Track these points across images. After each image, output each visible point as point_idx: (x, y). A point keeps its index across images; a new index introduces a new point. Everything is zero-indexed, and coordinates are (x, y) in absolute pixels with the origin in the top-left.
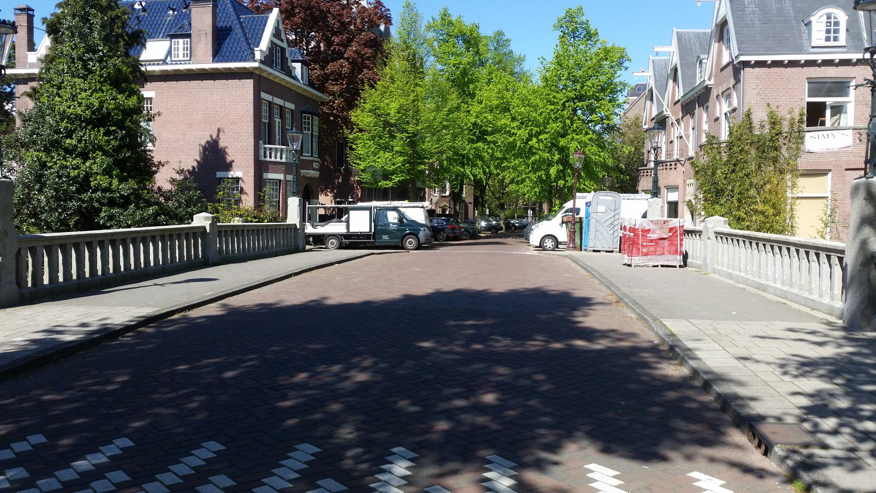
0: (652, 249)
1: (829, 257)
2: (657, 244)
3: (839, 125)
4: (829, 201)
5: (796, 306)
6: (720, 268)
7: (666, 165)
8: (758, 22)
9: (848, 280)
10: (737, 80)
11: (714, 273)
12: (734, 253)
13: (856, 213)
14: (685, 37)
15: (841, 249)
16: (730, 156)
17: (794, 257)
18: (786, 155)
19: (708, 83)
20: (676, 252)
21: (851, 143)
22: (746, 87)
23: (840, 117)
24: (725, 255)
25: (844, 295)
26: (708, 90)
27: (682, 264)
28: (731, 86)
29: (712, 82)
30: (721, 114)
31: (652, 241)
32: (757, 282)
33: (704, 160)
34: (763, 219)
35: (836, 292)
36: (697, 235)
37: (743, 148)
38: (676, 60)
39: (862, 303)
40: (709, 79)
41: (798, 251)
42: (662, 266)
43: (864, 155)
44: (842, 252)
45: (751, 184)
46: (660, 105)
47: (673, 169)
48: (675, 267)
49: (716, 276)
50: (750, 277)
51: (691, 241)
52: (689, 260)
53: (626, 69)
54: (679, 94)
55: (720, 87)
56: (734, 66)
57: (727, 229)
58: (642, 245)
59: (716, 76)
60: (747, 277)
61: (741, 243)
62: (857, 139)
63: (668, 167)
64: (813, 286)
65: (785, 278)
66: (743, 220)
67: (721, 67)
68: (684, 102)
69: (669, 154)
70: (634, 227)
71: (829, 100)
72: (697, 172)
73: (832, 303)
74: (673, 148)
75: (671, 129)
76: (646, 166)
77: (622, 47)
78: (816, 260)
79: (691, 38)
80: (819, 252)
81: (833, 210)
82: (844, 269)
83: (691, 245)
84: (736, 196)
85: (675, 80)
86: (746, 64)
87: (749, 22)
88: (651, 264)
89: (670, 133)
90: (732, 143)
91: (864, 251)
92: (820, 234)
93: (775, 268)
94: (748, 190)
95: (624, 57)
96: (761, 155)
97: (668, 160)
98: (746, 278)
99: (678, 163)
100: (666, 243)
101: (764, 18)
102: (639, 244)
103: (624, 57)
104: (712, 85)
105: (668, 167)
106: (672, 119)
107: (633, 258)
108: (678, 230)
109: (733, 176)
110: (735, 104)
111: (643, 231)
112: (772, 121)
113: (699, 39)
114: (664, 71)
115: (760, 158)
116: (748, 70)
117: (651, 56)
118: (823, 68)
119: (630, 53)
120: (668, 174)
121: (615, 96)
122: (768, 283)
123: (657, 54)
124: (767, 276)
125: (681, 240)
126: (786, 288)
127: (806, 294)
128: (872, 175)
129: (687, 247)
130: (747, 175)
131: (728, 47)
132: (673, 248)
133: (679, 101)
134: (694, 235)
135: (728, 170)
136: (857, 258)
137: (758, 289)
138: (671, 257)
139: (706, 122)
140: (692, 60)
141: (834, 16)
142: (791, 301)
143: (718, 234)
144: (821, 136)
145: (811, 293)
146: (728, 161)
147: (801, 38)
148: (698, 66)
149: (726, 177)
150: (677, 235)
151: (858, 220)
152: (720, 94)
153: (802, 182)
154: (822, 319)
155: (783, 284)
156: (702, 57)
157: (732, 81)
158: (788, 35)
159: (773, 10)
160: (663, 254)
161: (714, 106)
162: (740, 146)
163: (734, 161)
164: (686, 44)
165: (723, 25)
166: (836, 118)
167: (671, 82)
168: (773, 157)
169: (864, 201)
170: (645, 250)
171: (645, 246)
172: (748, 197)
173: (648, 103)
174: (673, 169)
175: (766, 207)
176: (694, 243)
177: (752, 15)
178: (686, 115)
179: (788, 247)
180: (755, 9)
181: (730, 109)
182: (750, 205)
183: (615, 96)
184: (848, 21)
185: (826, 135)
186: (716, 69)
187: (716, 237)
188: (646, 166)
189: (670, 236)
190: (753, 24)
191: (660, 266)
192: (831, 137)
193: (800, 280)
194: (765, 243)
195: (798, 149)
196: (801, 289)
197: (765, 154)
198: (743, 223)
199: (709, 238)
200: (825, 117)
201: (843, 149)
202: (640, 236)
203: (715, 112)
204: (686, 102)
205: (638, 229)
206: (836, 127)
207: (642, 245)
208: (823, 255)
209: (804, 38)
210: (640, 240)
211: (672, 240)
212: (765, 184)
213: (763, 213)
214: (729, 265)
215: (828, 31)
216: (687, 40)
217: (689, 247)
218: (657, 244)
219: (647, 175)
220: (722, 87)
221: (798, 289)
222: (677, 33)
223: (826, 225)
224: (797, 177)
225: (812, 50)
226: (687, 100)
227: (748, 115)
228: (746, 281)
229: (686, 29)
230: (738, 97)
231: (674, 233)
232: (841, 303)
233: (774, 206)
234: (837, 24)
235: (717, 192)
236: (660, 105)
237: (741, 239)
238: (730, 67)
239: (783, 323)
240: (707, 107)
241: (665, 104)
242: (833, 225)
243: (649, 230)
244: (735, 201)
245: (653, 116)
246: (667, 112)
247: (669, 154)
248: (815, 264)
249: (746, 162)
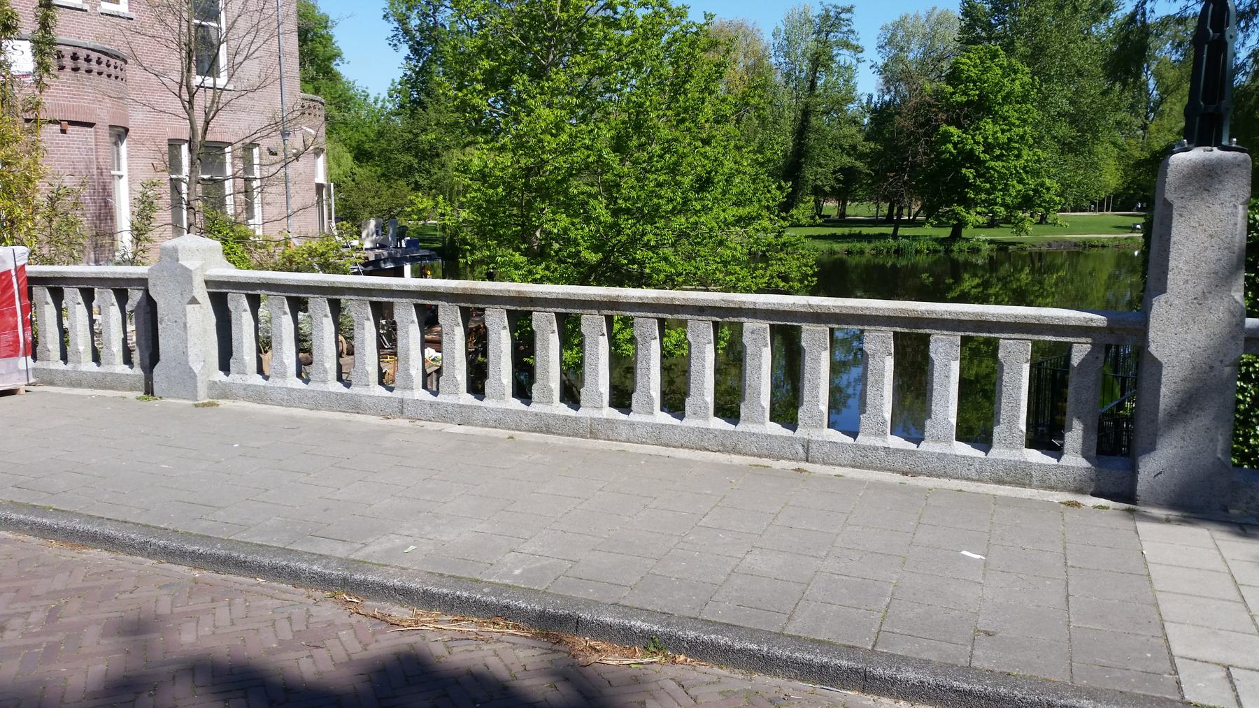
9: (1239, 147)
108: (14, 279)
150: (13, 296)
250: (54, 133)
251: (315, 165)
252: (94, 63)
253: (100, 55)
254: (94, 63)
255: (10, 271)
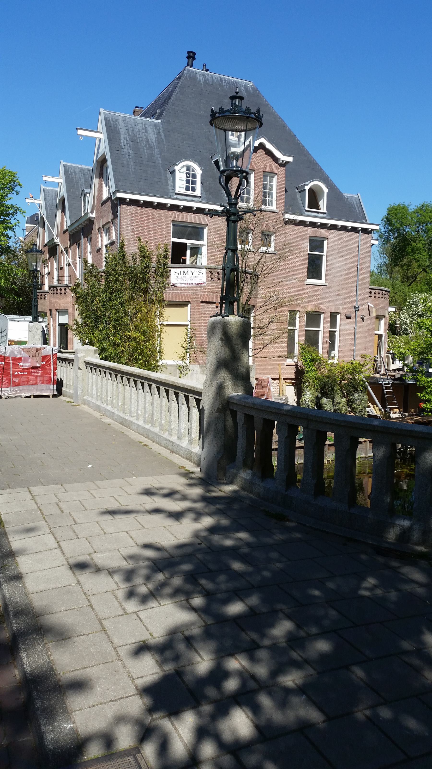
0: (24, 379)
1: (187, 398)
2: (29, 373)
3: (196, 263)
4: (189, 330)
5: (156, 448)
6: (89, 399)
7: (57, 290)
8: (132, 164)
9: (205, 426)
10: (115, 216)
11: (85, 404)
12: (102, 385)
13: (212, 354)
14: (72, 171)
15: (199, 391)
16: (107, 285)
17: (155, 394)
18: (155, 287)
19: (91, 215)
20: (49, 382)
21: (204, 280)
22: (122, 223)
23: (196, 259)
24: (94, 386)
25: (201, 440)
26: (91, 222)
27: (56, 393)
28: (110, 221)
29: (94, 215)
30: (102, 246)
31: (23, 370)
32: (122, 417)
33: (85, 288)
34: (135, 345)
35: (193, 436)
36: (70, 364)
37: (118, 278)
38: (63, 191)
39: (218, 452)
40: (92, 212)
41: (158, 388)
42: (35, 396)
43: (220, 291)
44: (200, 394)
45: (125, 312)
46: (50, 233)
47: (63, 294)
48: (49, 396)
49: (86, 408)
50: (115, 411)
51: (65, 369)
52: (64, 389)
53: (18, 193)
54: (67, 223)
55: (101, 220)
56: (112, 201)
57: (96, 360)
58: (13, 375)
59: (97, 209)
60: (113, 411)
61: (108, 375)
62: (209, 277)
63: (59, 292)
64: (173, 427)
65: (147, 416)
66: (119, 345)
67: (102, 202)
68: (71, 231)
69: (60, 279)
70: (3, 355)
71: (189, 242)
72: (78, 298)
73: (189, 447)
74: (63, 274)
75: (61, 257)
76: (41, 289)
77: (12, 171)
78: (175, 400)
79: (77, 172)
80: (178, 391)
81: (191, 338)
82: (201, 412)
83: (65, 372)
84: (113, 323)
85: (63, 210)
86: (122, 201)
87: (125, 162)
88: (23, 395)
89: (61, 260)
90: (108, 272)
91: (220, 396)
92: (181, 358)
93: (138, 404)
94: (122, 317)
95: (15, 181)
96: (133, 286)
97: (59, 285)
98: (112, 412)
99: (67, 288)
100: (39, 372)
101: (137, 161)
102: (9, 374)
103: (15, 181)
104: (94, 218)
105: (59, 292)
106: (62, 247)
107: (3, 389)
108: (52, 358)
109: (110, 303)
110: (114, 238)
111: (14, 359)
112: (143, 254)
113: (84, 174)
114: (54, 201)
115: (133, 288)
116: (124, 207)
117: (42, 185)
118: (184, 213)
119: (21, 178)
120: (58, 298)
121: (7, 218)
122: (131, 419)
123: (46, 182)
124: (130, 412)
125: (55, 369)
126: (148, 426)
127: (166, 435)
128: (228, 314)
129: (62, 375)
130: (121, 304)
131: (107, 184)
132: (46, 378)
133: (66, 230)
134: (67, 363)
135: (106, 298)
136: (213, 404)
137: (123, 425)
138: (44, 387)
139: (90, 252)
140: (77, 193)
141: (192, 169)
142: (153, 441)
143: (88, 364)
144: (182, 272)
145: (171, 434)
146: (105, 289)
147: (167, 184)
148: (83, 200)
149: (104, 304)
150: (51, 363)
151: (214, 362)
152: (101, 227)
153: (167, 311)
154: (180, 468)
155: (145, 422)
156: (86, 191)
157: (111, 216)
158: (157, 180)
159: (145, 155)
160: (36, 384)
161: (97, 239)
162: (115, 276)
163: (110, 290)
164: (72, 178)
165: (102, 162)
166: (194, 257)
167: (59, 212)
168: (143, 288)
169: (220, 341)
170: (16, 380)
171: (16, 375)
172: (122, 324)
173: (41, 230)
174: (63, 294)
175: (138, 335)
176: (68, 372)
177: (127, 156)
178: (73, 244)
179: (150, 383)
180: (130, 151)
181: (109, 242)
182: (124, 332)
183: (7, 218)
184: (202, 174)
185: (186, 272)
186: (97, 203)
187: (87, 367)
188: (41, 289)
189: (43, 365)
190: (128, 165)
191: (32, 397)
192: (190, 273)
193: (161, 419)
194: (129, 377)
195: (164, 282)
196: (161, 429)
197: (137, 285)
198: (118, 348)
199: (79, 368)
200: (186, 257)
201: (199, 285)
202: (11, 365)
203: (97, 243)
204: (73, 232)
205: (8, 357)
206: (194, 265)
207: (13, 375)
208: (181, 395)
209: (170, 184)
210: (11, 369)
211: (45, 369)
212: (137, 312)
213: (135, 339)
214: (97, 396)
215: (188, 182)
216: (74, 174)
217: (63, 375)
218: (29, 373)
219: (41, 298)
220: (102, 221)
221: (158, 428)
222: (64, 166)
223: (186, 351)
224: (163, 307)
225: (176, 196)
226: (73, 230)
227: (122, 248)
228: (111, 415)
229: (72, 163)
230: (116, 231)
231: (46, 362)
232: (198, 447)
233: (144, 333)
234: (194, 176)
235: (96, 318)
236: (50, 233)
237: (107, 371)
238: (109, 203)
239: (141, 479)
240: (91, 238)
241: (55, 234)
242: (192, 351)
243: (20, 359)
244: (111, 328)
245: (46, 242)
246: (57, 240)
247: (60, 279)
248: (174, 404)
249: (120, 291)
250: (213, 307)
251: (379, 324)
252: (373, 293)
253: (379, 291)
254: (381, 294)
255: (50, 355)
